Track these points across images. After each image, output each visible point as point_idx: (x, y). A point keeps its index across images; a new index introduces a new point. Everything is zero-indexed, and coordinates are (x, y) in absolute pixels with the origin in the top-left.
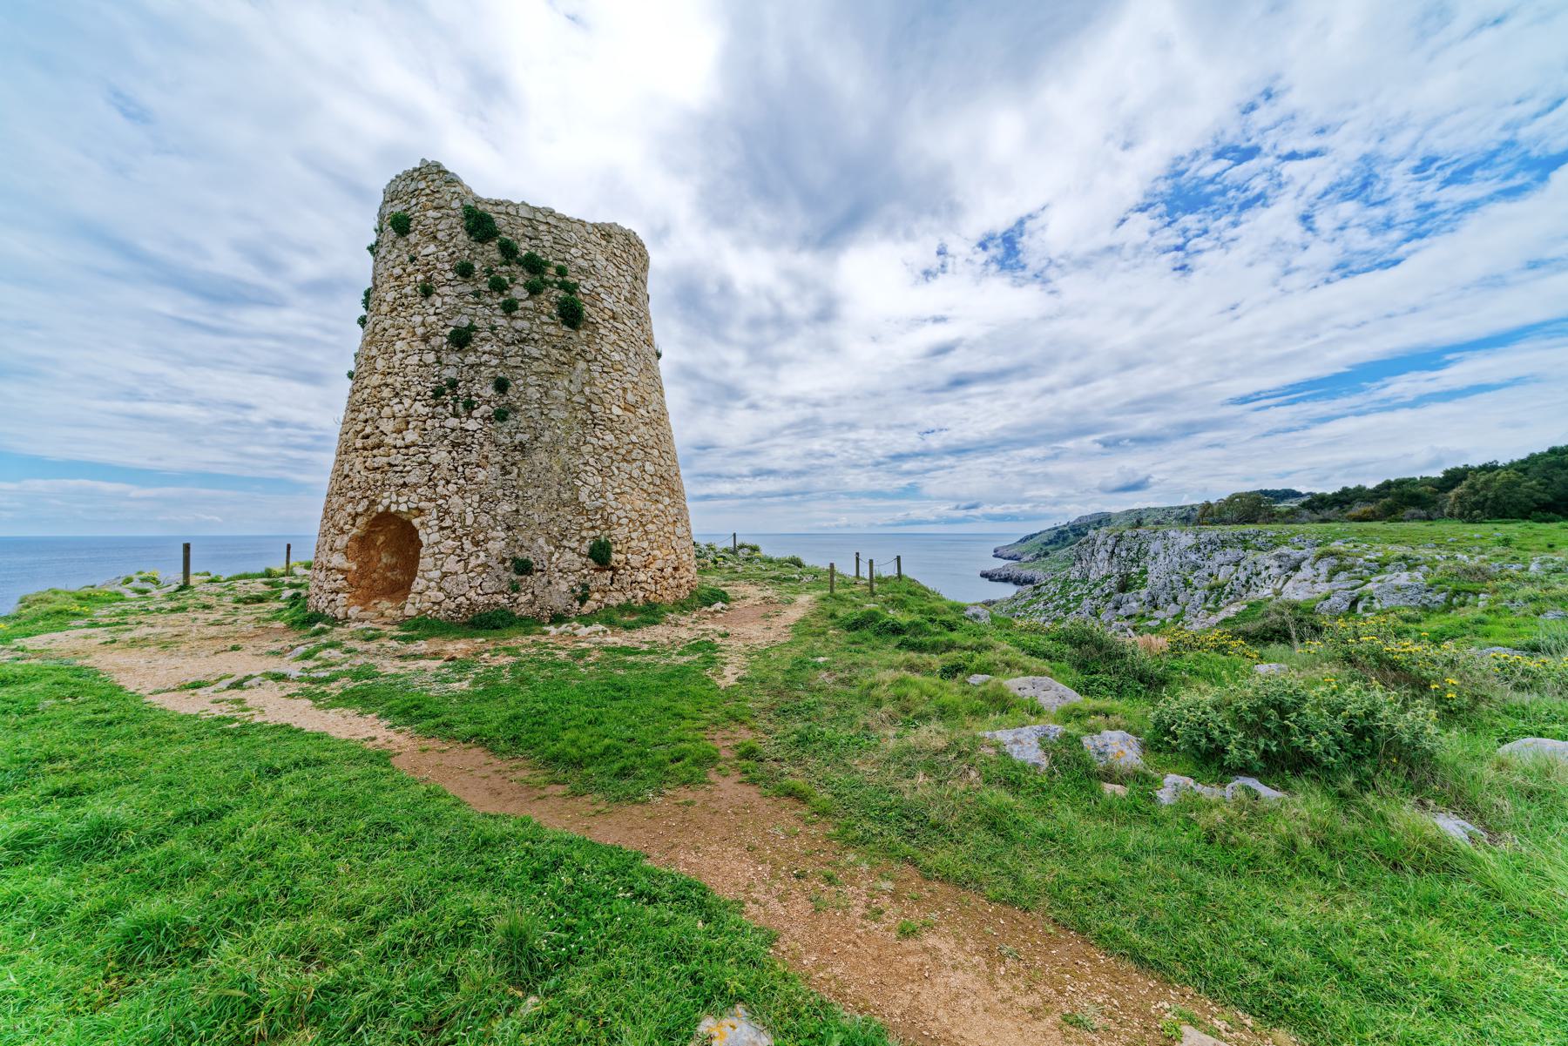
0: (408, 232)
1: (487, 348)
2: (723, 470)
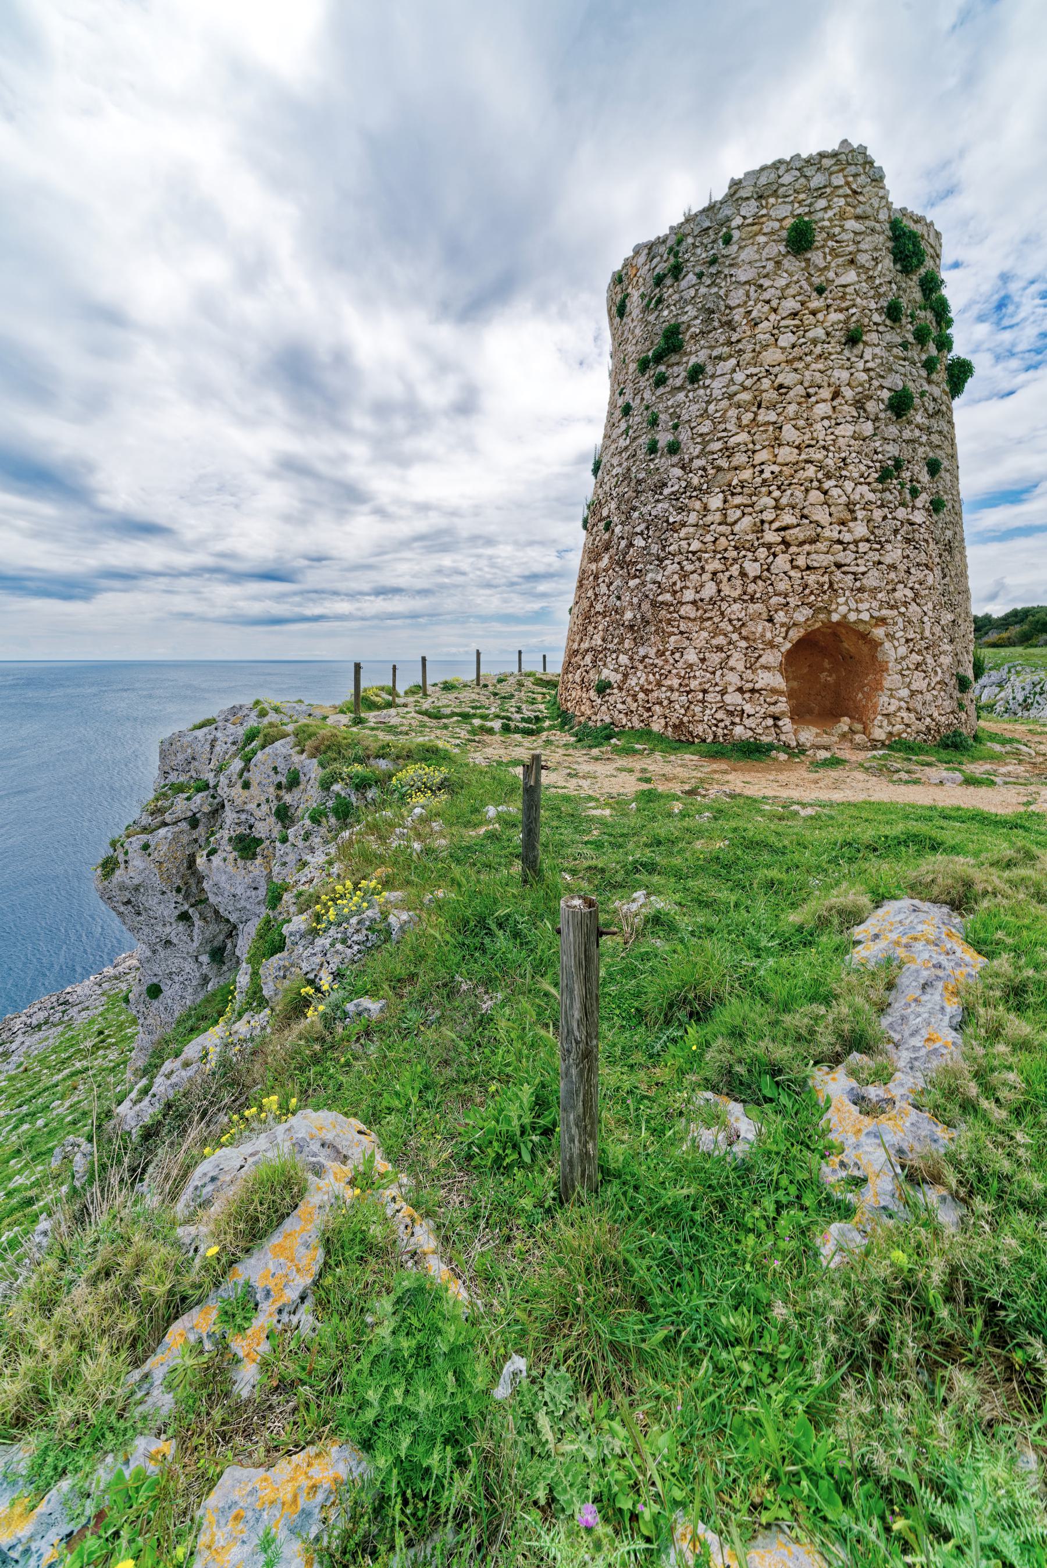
0: (807, 249)
2: (341, 586)
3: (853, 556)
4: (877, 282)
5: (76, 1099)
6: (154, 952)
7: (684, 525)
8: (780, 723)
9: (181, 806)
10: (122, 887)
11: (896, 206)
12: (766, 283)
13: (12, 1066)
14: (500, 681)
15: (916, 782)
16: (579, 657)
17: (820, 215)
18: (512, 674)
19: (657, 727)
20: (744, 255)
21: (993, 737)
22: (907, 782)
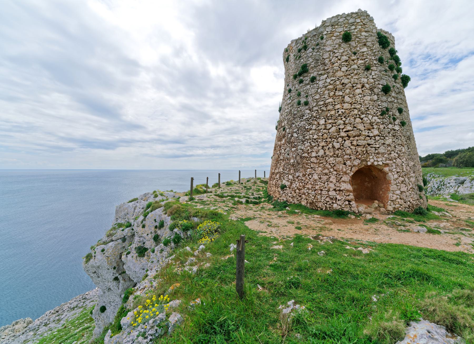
3: (374, 141)
4: (374, 51)
5: (83, 341)
6: (104, 293)
7: (311, 129)
8: (351, 203)
9: (120, 233)
10: (93, 267)
11: (379, 28)
12: (336, 51)
13: (61, 325)
14: (248, 181)
15: (408, 231)
16: (275, 175)
17: (353, 31)
18: (253, 178)
19: (303, 203)
20: (328, 43)
21: (434, 208)
22: (404, 231)
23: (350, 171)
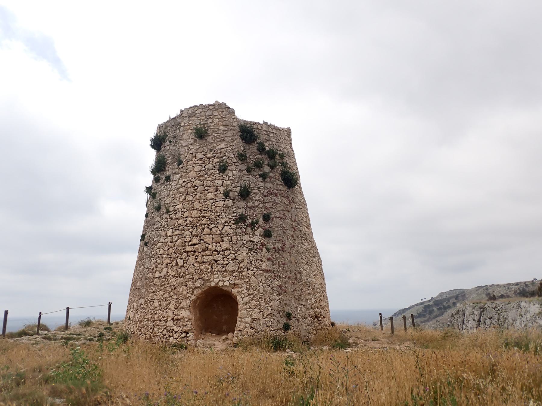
1: (257, 198)
23: (192, 294)
